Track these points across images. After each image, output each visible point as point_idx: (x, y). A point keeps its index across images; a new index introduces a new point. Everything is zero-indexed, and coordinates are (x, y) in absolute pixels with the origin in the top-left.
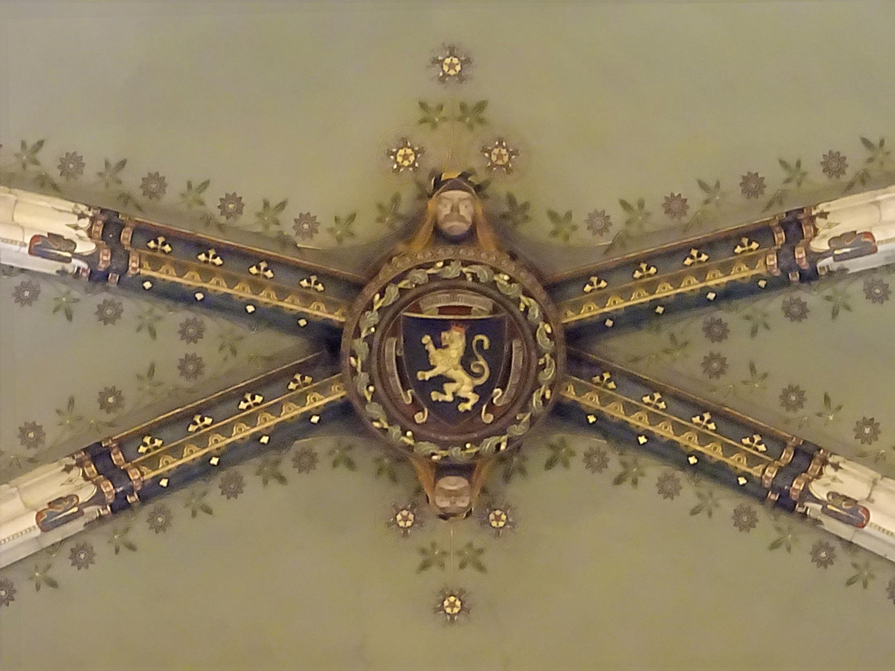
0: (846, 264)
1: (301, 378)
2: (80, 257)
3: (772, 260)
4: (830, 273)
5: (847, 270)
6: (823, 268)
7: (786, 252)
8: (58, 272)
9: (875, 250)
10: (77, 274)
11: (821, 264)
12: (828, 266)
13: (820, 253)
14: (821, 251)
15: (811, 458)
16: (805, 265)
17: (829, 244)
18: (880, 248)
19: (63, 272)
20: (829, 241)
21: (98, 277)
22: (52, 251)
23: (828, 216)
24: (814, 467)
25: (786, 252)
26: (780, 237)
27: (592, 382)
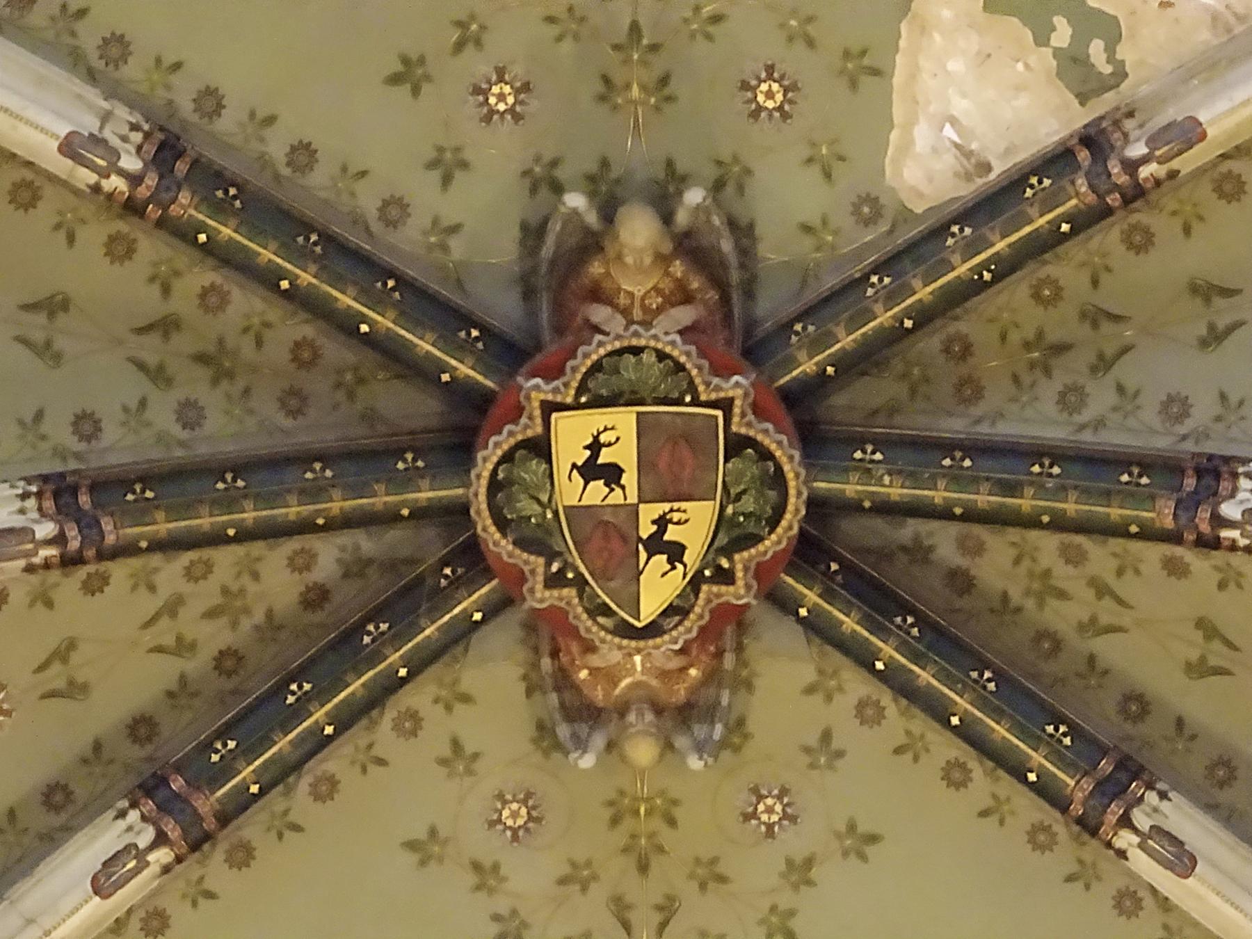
0: (1175, 164)
1: (413, 459)
2: (122, 173)
3: (1082, 185)
4: (1158, 183)
5: (1179, 172)
6: (1146, 179)
7: (1098, 174)
8: (89, 186)
9: (1203, 136)
10: (110, 196)
11: (1145, 172)
12: (1152, 175)
13: (1230, 521)
14: (1234, 520)
15: (1217, 476)
16: (1123, 179)
17: (1243, 515)
18: (1211, 132)
19: (96, 189)
20: (1244, 511)
21: (70, 562)
22: (89, 155)
23: (1136, 114)
24: (1225, 486)
25: (1098, 174)
26: (1084, 156)
27: (893, 623)
